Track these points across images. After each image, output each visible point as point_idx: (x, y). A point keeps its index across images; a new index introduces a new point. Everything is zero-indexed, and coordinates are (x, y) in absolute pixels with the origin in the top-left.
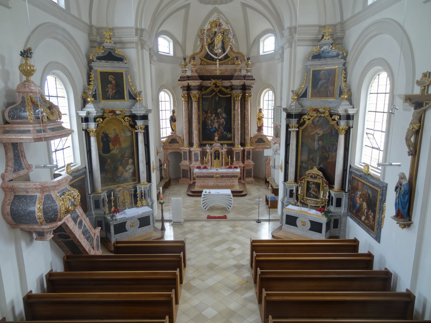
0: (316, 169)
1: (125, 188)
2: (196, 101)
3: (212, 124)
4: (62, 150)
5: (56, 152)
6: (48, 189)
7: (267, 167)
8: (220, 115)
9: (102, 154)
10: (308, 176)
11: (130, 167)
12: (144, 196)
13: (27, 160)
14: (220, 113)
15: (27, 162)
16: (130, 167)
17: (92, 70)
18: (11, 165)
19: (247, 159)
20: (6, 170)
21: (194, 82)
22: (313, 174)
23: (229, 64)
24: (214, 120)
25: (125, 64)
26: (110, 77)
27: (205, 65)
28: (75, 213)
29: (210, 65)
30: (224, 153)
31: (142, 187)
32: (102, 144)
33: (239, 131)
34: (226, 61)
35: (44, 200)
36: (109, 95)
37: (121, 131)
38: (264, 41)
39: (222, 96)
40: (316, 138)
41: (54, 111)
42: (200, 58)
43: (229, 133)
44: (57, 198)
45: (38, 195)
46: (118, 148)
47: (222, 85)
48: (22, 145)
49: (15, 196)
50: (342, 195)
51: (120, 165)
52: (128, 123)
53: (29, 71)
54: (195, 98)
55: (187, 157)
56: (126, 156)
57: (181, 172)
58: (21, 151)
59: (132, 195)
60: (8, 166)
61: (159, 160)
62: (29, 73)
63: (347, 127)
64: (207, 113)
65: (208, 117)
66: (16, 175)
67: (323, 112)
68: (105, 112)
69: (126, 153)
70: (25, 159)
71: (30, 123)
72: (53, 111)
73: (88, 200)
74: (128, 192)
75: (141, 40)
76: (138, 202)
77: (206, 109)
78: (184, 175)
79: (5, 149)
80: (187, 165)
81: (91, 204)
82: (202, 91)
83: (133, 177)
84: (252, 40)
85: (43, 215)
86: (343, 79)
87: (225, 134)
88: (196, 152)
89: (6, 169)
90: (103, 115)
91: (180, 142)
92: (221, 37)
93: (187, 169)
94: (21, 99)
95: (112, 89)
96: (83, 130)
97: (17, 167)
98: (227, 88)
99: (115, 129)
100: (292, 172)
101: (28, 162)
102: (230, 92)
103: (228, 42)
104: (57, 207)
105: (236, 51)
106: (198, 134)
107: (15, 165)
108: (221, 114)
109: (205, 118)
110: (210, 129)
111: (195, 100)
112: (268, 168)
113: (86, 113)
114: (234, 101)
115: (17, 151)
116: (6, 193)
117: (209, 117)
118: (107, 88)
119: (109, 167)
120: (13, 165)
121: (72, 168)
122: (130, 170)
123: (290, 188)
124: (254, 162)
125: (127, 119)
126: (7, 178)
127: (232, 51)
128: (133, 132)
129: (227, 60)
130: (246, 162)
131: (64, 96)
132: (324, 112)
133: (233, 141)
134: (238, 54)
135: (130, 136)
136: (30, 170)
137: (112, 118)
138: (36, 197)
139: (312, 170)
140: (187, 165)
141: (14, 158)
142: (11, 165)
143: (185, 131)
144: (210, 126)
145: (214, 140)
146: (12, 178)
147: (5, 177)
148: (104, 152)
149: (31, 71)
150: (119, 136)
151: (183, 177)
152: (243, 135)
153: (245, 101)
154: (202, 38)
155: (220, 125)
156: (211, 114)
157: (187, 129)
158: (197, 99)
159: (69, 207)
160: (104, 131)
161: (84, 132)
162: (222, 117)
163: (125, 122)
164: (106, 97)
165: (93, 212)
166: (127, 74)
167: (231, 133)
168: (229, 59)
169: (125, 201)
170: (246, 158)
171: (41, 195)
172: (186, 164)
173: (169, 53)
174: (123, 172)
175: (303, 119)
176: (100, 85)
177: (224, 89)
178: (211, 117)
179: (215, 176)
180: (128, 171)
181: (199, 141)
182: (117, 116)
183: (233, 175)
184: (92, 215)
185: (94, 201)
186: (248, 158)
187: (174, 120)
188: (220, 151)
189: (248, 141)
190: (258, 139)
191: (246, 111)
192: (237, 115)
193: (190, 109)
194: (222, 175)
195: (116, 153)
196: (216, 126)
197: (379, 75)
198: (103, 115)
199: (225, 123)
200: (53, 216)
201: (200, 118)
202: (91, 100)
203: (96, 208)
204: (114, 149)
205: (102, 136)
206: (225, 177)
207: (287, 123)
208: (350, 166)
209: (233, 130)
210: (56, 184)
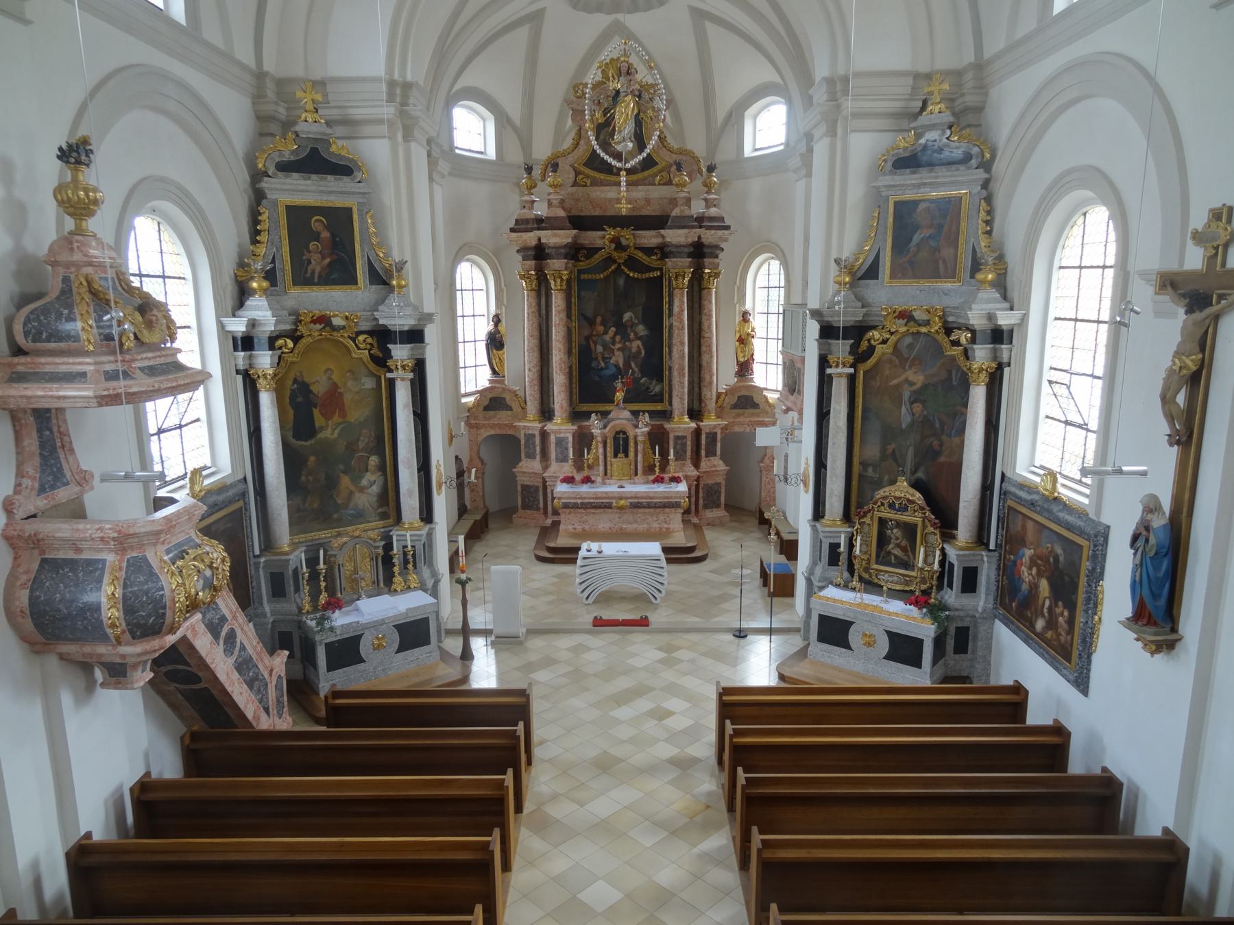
0: (905, 483)
1: (358, 539)
2: (561, 290)
3: (606, 356)
4: (178, 430)
5: (162, 435)
6: (136, 540)
7: (764, 479)
8: (629, 329)
9: (293, 441)
10: (883, 504)
11: (373, 478)
12: (411, 560)
13: (77, 459)
14: (630, 323)
15: (79, 463)
16: (373, 478)
17: (264, 202)
18: (31, 472)
19: (707, 456)
20: (19, 488)
21: (556, 235)
22: (895, 497)
23: (657, 182)
24: (614, 345)
25: (359, 182)
26: (316, 221)
27: (586, 186)
28: (214, 609)
29: (602, 186)
30: (640, 438)
31: (406, 536)
32: (291, 412)
33: (684, 374)
34: (646, 173)
35: (126, 573)
36: (313, 272)
37: (348, 374)
38: (755, 118)
39: (636, 276)
40: (906, 395)
41: (154, 318)
42: (572, 166)
43: (654, 382)
44: (163, 568)
45: (110, 558)
46: (339, 424)
47: (634, 244)
48: (64, 415)
49: (44, 561)
50: (979, 557)
51: (345, 472)
52: (367, 351)
53: (84, 203)
54: (559, 281)
55: (535, 450)
56: (361, 447)
57: (519, 494)
58: (59, 432)
59: (377, 558)
60: (23, 477)
61: (457, 457)
62: (84, 208)
63: (994, 365)
64: (591, 322)
65: (595, 336)
66: (45, 502)
67: (923, 321)
68: (300, 321)
69: (362, 438)
70: (71, 454)
71: (87, 354)
72: (151, 317)
73: (253, 573)
74: (365, 550)
75: (402, 114)
76: (395, 580)
77: (589, 314)
78: (527, 500)
79: (14, 426)
80: (536, 471)
81: (260, 583)
82: (578, 260)
83: (380, 506)
84: (721, 115)
85: (122, 616)
86: (981, 225)
87: (644, 385)
88: (562, 435)
89: (18, 485)
90: (296, 330)
91: (515, 405)
92: (632, 106)
93: (536, 484)
94: (60, 282)
95: (319, 255)
96: (238, 372)
97: (50, 478)
98: (649, 251)
99: (330, 369)
100: (835, 493)
101: (81, 464)
102: (659, 262)
103: (651, 119)
104: (162, 592)
105: (675, 147)
106: (567, 384)
107: (43, 471)
108: (632, 326)
109: (587, 338)
110: (602, 369)
111: (559, 288)
112: (767, 480)
113: (246, 323)
114: (669, 290)
115: (48, 433)
116: (17, 553)
117: (598, 335)
118: (305, 252)
119: (311, 479)
120: (36, 472)
121: (207, 482)
122: (371, 486)
123: (830, 537)
124: (726, 463)
125: (364, 341)
126: (21, 510)
127: (665, 147)
128: (380, 377)
129: (650, 172)
130: (705, 464)
131: (182, 276)
132: (929, 321)
133: (667, 404)
134: (681, 154)
135: (373, 389)
136: (87, 488)
137: (320, 337)
138: (104, 565)
139: (892, 488)
140: (536, 474)
141: (40, 454)
142: (31, 472)
143: (531, 374)
144: (601, 362)
145: (613, 402)
146: (33, 510)
147: (15, 508)
148: (297, 436)
149: (88, 204)
150: (341, 391)
151: (524, 508)
152: (696, 385)
153: (701, 289)
154: (578, 110)
155: (629, 357)
156: (605, 327)
157: (534, 370)
158: (565, 282)
159: (197, 594)
160: (298, 374)
161: (239, 378)
162: (636, 334)
163: (359, 348)
164: (302, 278)
165: (267, 608)
166: (364, 212)
167: (661, 380)
168: (655, 169)
169: (357, 576)
170: (703, 453)
171: (118, 558)
172: (532, 471)
173: (483, 150)
174: (351, 493)
175: (869, 341)
176: (286, 242)
177: (640, 254)
178: (603, 334)
179: (614, 504)
180: (365, 491)
181: (571, 405)
182: (335, 334)
183: (666, 500)
184: (264, 615)
185: (268, 575)
186: (711, 453)
187: (498, 345)
188: (631, 433)
189: (711, 405)
190: (739, 397)
191: (704, 318)
192: (678, 329)
193: (543, 312)
194: (636, 501)
195: (332, 437)
196: (617, 362)
197: (1085, 214)
198: (296, 330)
199: (643, 352)
200: (153, 618)
201: (574, 339)
202: (260, 286)
203: (274, 596)
204: (327, 426)
205: (292, 390)
206: (644, 507)
207: (823, 352)
208: (1003, 475)
209: (667, 373)
210: (160, 528)
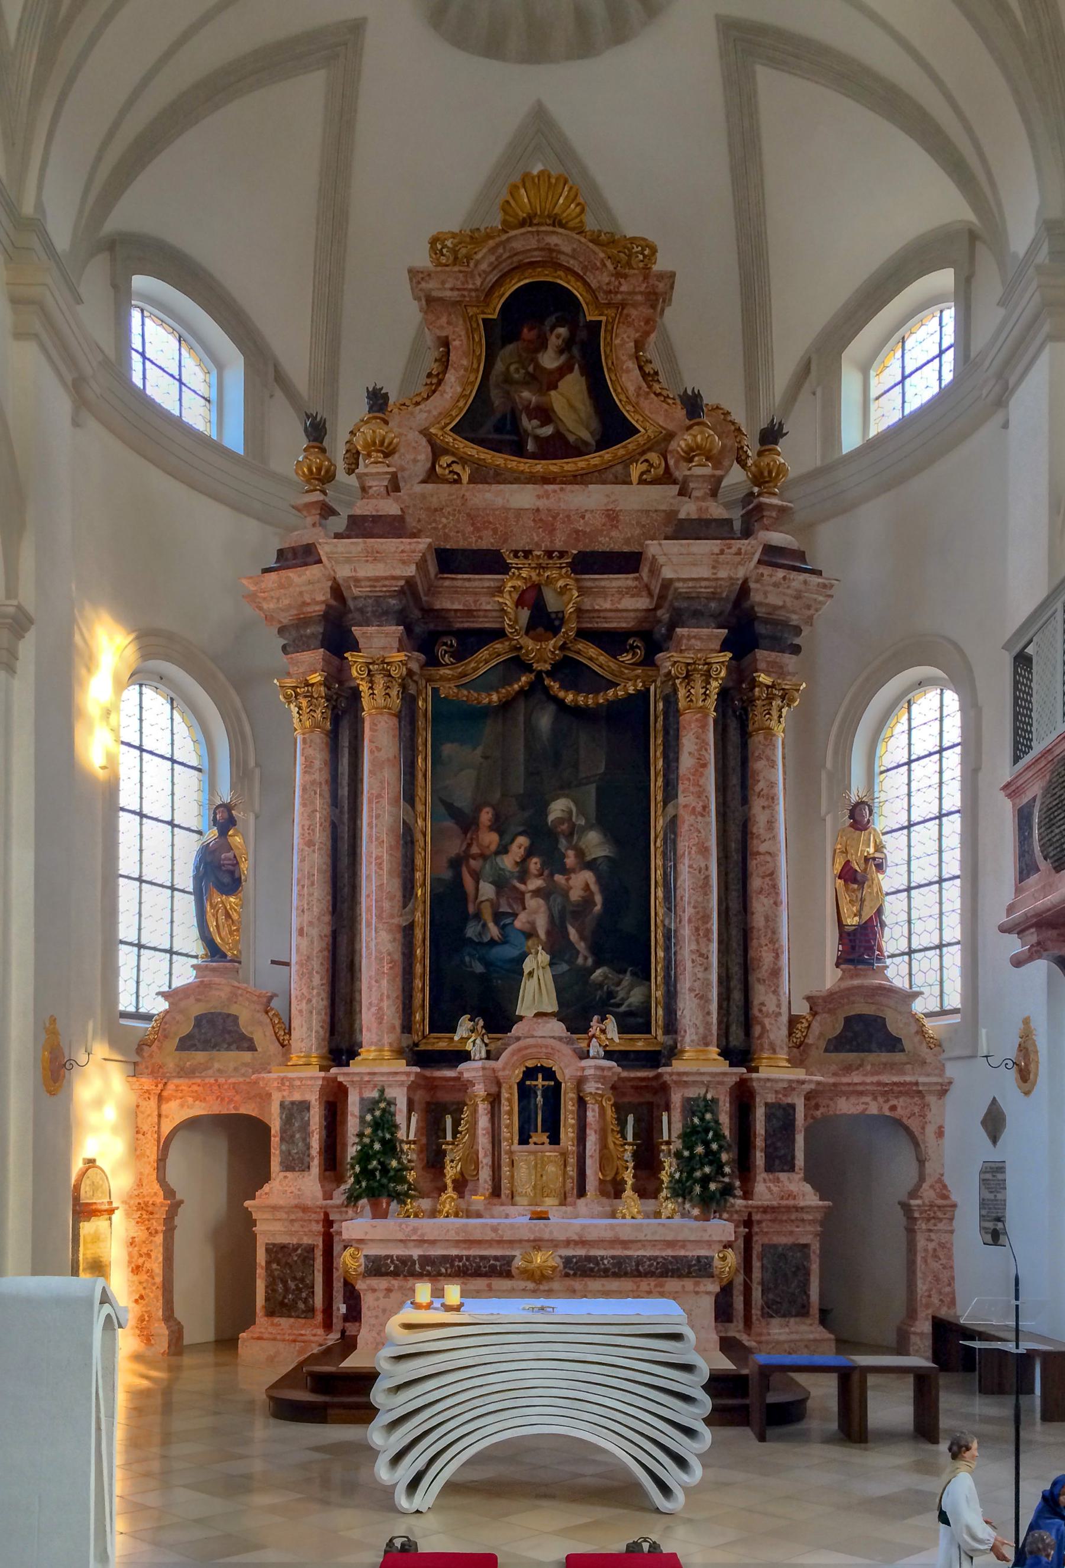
3: (504, 908)
7: (921, 1242)
8: (563, 843)
14: (565, 827)
19: (769, 1168)
21: (375, 557)
27: (458, 481)
30: (591, 1087)
33: (708, 931)
34: (607, 455)
38: (865, 370)
42: (425, 432)
43: (627, 979)
54: (380, 681)
55: (308, 1147)
57: (260, 1272)
64: (467, 824)
77: (463, 799)
80: (309, 1203)
87: (600, 986)
91: (263, 1037)
106: (398, 956)
108: (571, 834)
109: (456, 864)
110: (493, 943)
112: (931, 1246)
117: (483, 857)
124: (823, 1193)
129: (619, 450)
140: (305, 1209)
143: (305, 942)
153: (745, 735)
154: (440, 300)
156: (501, 834)
157: (315, 932)
162: (580, 853)
167: (644, 974)
168: (631, 443)
177: (592, 651)
178: (498, 853)
179: (518, 1263)
181: (407, 1027)
183: (669, 1252)
187: (226, 879)
188: (567, 1068)
189: (777, 1032)
190: (848, 1020)
191: (757, 806)
193: (344, 791)
194: (581, 1252)
196: (533, 924)
199: (598, 898)
201: (419, 862)
206: (606, 1273)
209: (661, 954)
